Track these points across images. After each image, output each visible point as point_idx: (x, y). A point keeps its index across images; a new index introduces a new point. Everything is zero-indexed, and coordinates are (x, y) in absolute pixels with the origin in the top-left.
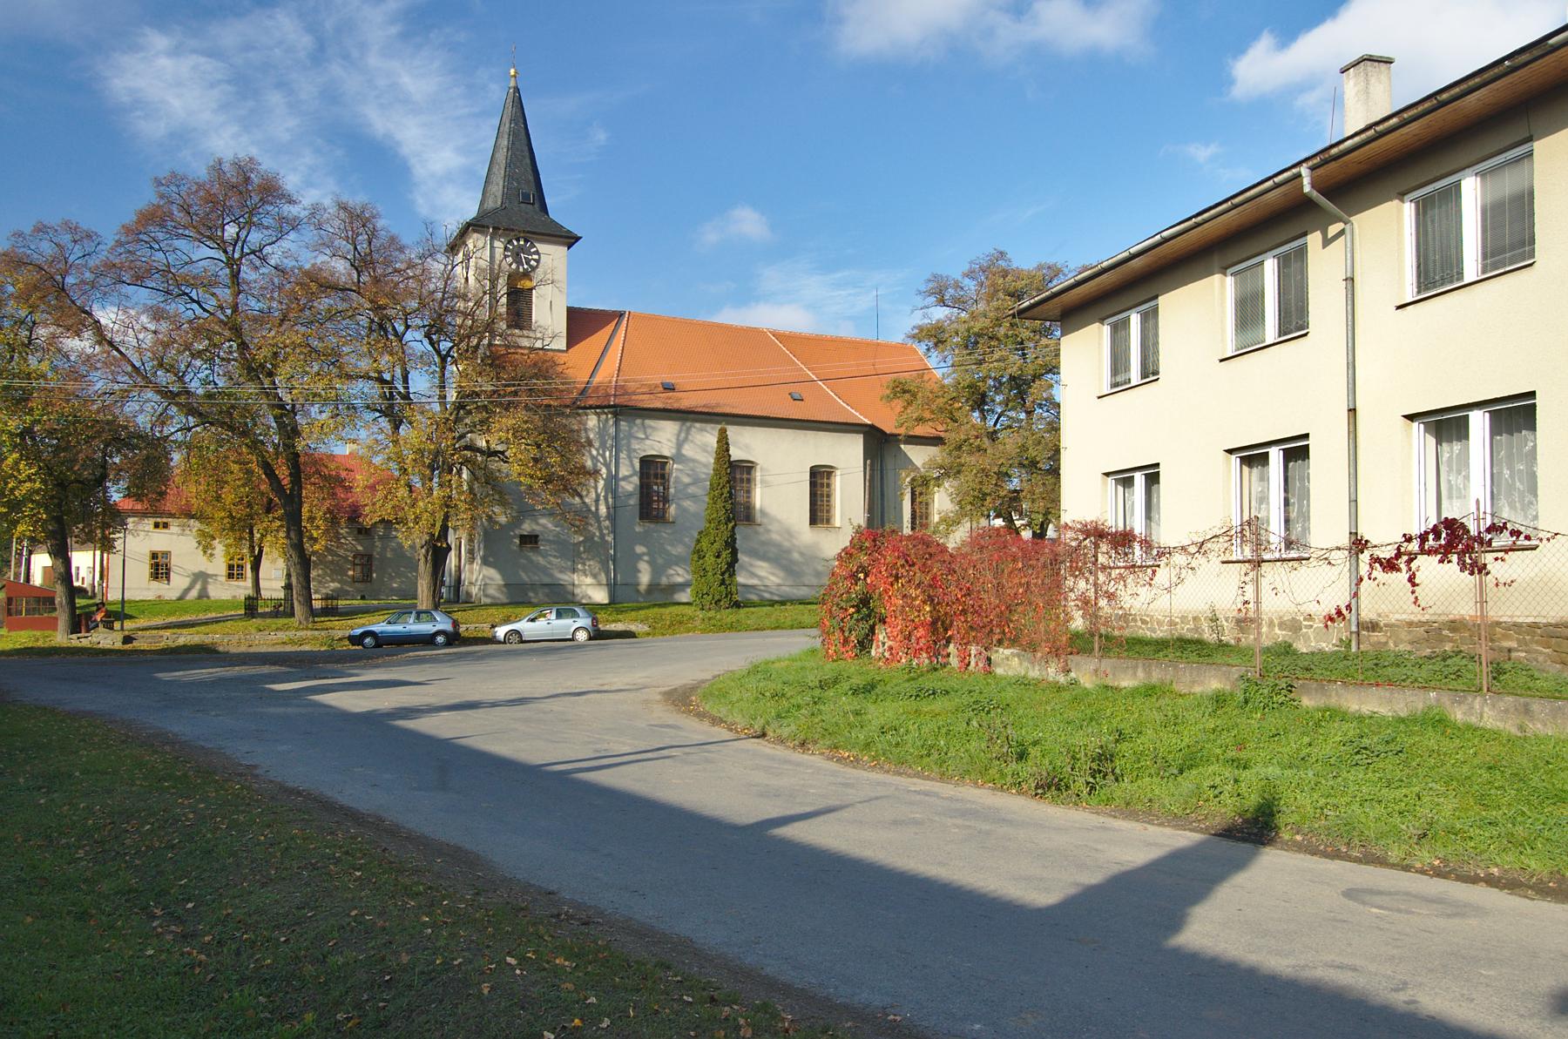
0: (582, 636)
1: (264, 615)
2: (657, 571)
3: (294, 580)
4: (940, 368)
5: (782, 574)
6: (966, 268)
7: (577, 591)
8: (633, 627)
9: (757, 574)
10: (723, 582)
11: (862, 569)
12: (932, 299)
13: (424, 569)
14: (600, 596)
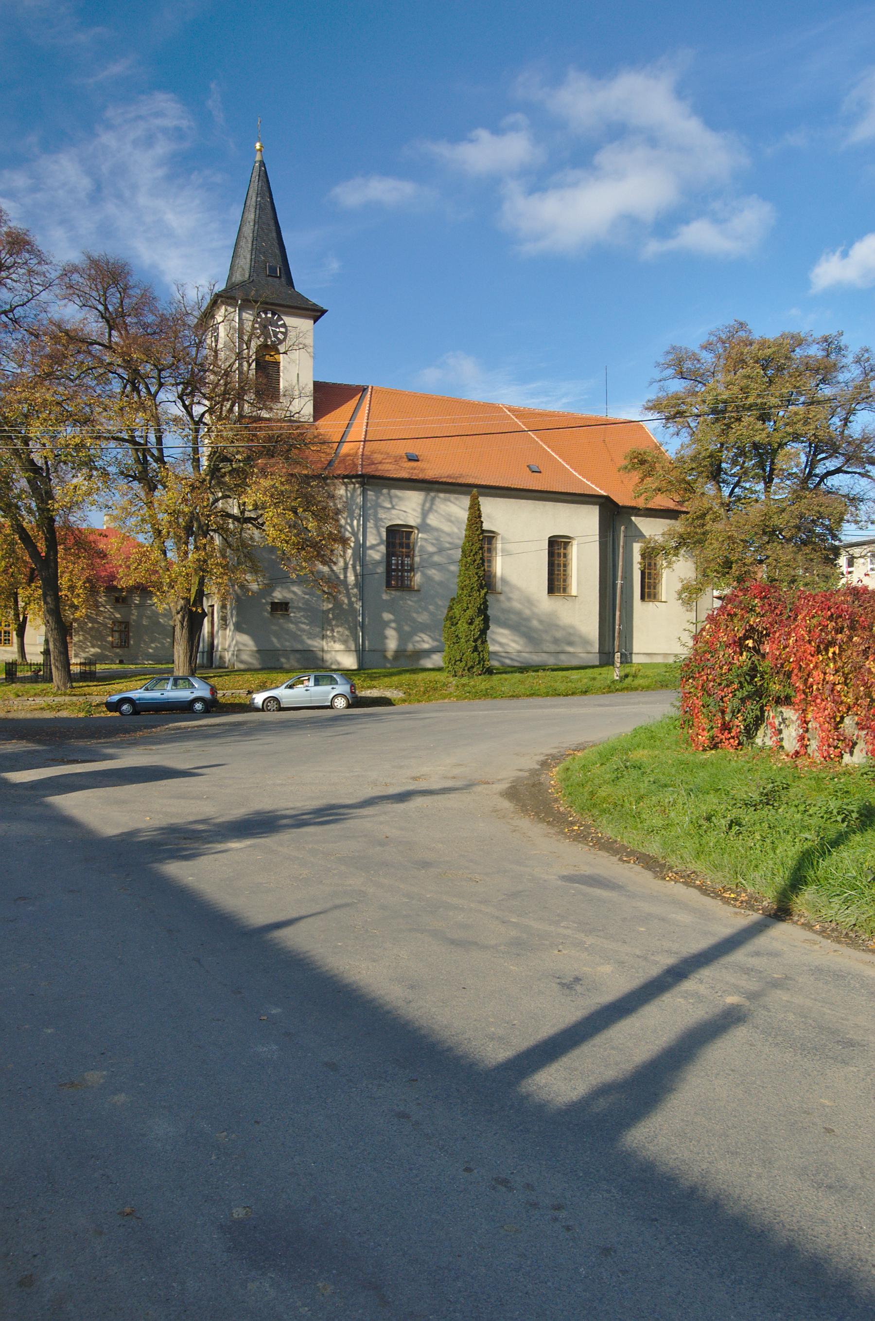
0: (340, 703)
1: (24, 680)
2: (403, 638)
3: (51, 646)
4: (673, 443)
5: (522, 641)
6: (703, 341)
7: (327, 657)
8: (388, 694)
9: (504, 642)
10: (475, 649)
11: (751, 631)
12: (670, 372)
13: (181, 635)
14: (349, 662)
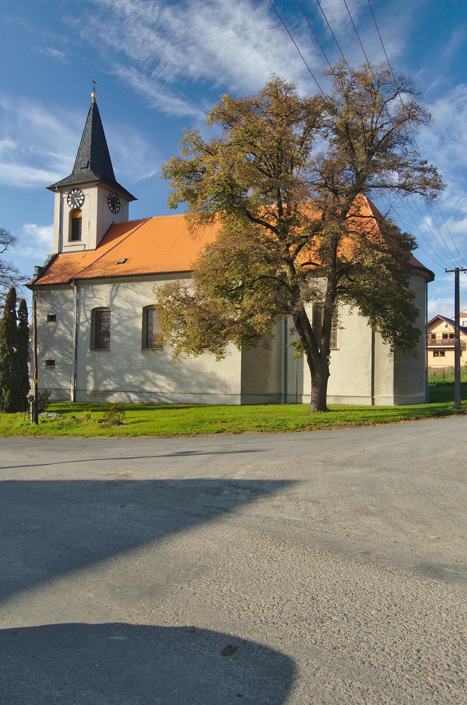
2: (98, 382)
5: (174, 384)
